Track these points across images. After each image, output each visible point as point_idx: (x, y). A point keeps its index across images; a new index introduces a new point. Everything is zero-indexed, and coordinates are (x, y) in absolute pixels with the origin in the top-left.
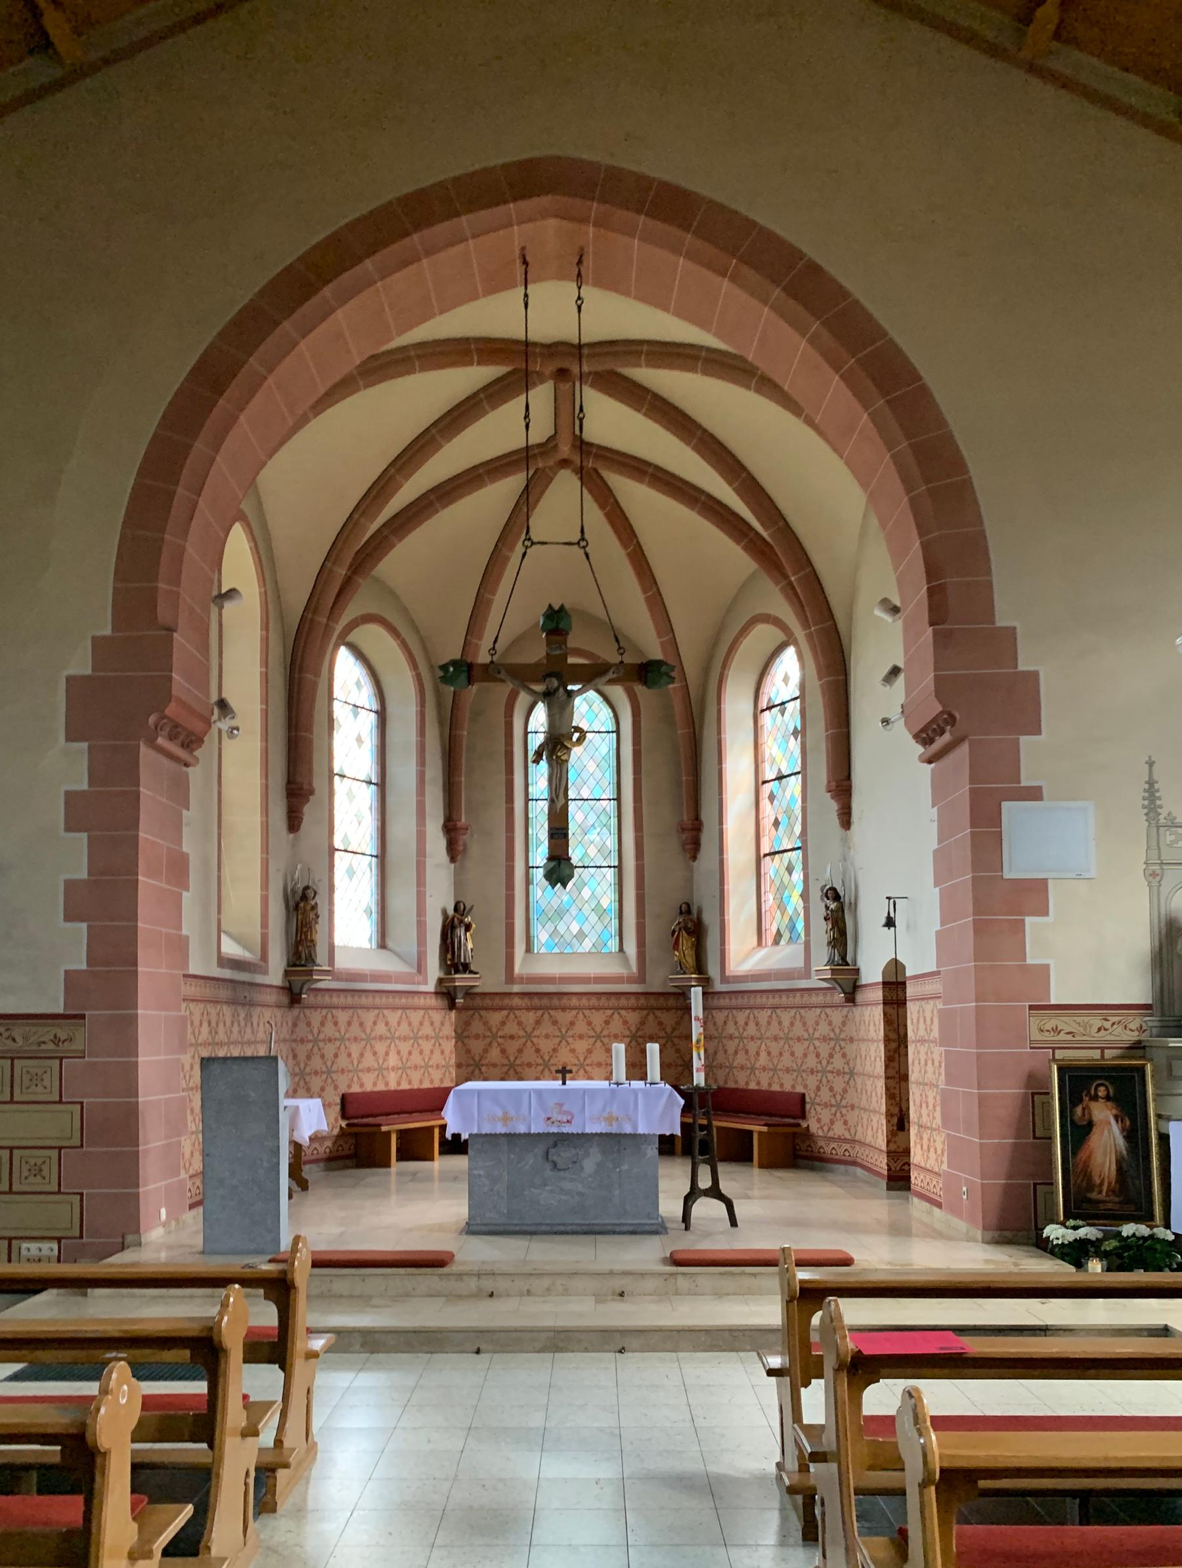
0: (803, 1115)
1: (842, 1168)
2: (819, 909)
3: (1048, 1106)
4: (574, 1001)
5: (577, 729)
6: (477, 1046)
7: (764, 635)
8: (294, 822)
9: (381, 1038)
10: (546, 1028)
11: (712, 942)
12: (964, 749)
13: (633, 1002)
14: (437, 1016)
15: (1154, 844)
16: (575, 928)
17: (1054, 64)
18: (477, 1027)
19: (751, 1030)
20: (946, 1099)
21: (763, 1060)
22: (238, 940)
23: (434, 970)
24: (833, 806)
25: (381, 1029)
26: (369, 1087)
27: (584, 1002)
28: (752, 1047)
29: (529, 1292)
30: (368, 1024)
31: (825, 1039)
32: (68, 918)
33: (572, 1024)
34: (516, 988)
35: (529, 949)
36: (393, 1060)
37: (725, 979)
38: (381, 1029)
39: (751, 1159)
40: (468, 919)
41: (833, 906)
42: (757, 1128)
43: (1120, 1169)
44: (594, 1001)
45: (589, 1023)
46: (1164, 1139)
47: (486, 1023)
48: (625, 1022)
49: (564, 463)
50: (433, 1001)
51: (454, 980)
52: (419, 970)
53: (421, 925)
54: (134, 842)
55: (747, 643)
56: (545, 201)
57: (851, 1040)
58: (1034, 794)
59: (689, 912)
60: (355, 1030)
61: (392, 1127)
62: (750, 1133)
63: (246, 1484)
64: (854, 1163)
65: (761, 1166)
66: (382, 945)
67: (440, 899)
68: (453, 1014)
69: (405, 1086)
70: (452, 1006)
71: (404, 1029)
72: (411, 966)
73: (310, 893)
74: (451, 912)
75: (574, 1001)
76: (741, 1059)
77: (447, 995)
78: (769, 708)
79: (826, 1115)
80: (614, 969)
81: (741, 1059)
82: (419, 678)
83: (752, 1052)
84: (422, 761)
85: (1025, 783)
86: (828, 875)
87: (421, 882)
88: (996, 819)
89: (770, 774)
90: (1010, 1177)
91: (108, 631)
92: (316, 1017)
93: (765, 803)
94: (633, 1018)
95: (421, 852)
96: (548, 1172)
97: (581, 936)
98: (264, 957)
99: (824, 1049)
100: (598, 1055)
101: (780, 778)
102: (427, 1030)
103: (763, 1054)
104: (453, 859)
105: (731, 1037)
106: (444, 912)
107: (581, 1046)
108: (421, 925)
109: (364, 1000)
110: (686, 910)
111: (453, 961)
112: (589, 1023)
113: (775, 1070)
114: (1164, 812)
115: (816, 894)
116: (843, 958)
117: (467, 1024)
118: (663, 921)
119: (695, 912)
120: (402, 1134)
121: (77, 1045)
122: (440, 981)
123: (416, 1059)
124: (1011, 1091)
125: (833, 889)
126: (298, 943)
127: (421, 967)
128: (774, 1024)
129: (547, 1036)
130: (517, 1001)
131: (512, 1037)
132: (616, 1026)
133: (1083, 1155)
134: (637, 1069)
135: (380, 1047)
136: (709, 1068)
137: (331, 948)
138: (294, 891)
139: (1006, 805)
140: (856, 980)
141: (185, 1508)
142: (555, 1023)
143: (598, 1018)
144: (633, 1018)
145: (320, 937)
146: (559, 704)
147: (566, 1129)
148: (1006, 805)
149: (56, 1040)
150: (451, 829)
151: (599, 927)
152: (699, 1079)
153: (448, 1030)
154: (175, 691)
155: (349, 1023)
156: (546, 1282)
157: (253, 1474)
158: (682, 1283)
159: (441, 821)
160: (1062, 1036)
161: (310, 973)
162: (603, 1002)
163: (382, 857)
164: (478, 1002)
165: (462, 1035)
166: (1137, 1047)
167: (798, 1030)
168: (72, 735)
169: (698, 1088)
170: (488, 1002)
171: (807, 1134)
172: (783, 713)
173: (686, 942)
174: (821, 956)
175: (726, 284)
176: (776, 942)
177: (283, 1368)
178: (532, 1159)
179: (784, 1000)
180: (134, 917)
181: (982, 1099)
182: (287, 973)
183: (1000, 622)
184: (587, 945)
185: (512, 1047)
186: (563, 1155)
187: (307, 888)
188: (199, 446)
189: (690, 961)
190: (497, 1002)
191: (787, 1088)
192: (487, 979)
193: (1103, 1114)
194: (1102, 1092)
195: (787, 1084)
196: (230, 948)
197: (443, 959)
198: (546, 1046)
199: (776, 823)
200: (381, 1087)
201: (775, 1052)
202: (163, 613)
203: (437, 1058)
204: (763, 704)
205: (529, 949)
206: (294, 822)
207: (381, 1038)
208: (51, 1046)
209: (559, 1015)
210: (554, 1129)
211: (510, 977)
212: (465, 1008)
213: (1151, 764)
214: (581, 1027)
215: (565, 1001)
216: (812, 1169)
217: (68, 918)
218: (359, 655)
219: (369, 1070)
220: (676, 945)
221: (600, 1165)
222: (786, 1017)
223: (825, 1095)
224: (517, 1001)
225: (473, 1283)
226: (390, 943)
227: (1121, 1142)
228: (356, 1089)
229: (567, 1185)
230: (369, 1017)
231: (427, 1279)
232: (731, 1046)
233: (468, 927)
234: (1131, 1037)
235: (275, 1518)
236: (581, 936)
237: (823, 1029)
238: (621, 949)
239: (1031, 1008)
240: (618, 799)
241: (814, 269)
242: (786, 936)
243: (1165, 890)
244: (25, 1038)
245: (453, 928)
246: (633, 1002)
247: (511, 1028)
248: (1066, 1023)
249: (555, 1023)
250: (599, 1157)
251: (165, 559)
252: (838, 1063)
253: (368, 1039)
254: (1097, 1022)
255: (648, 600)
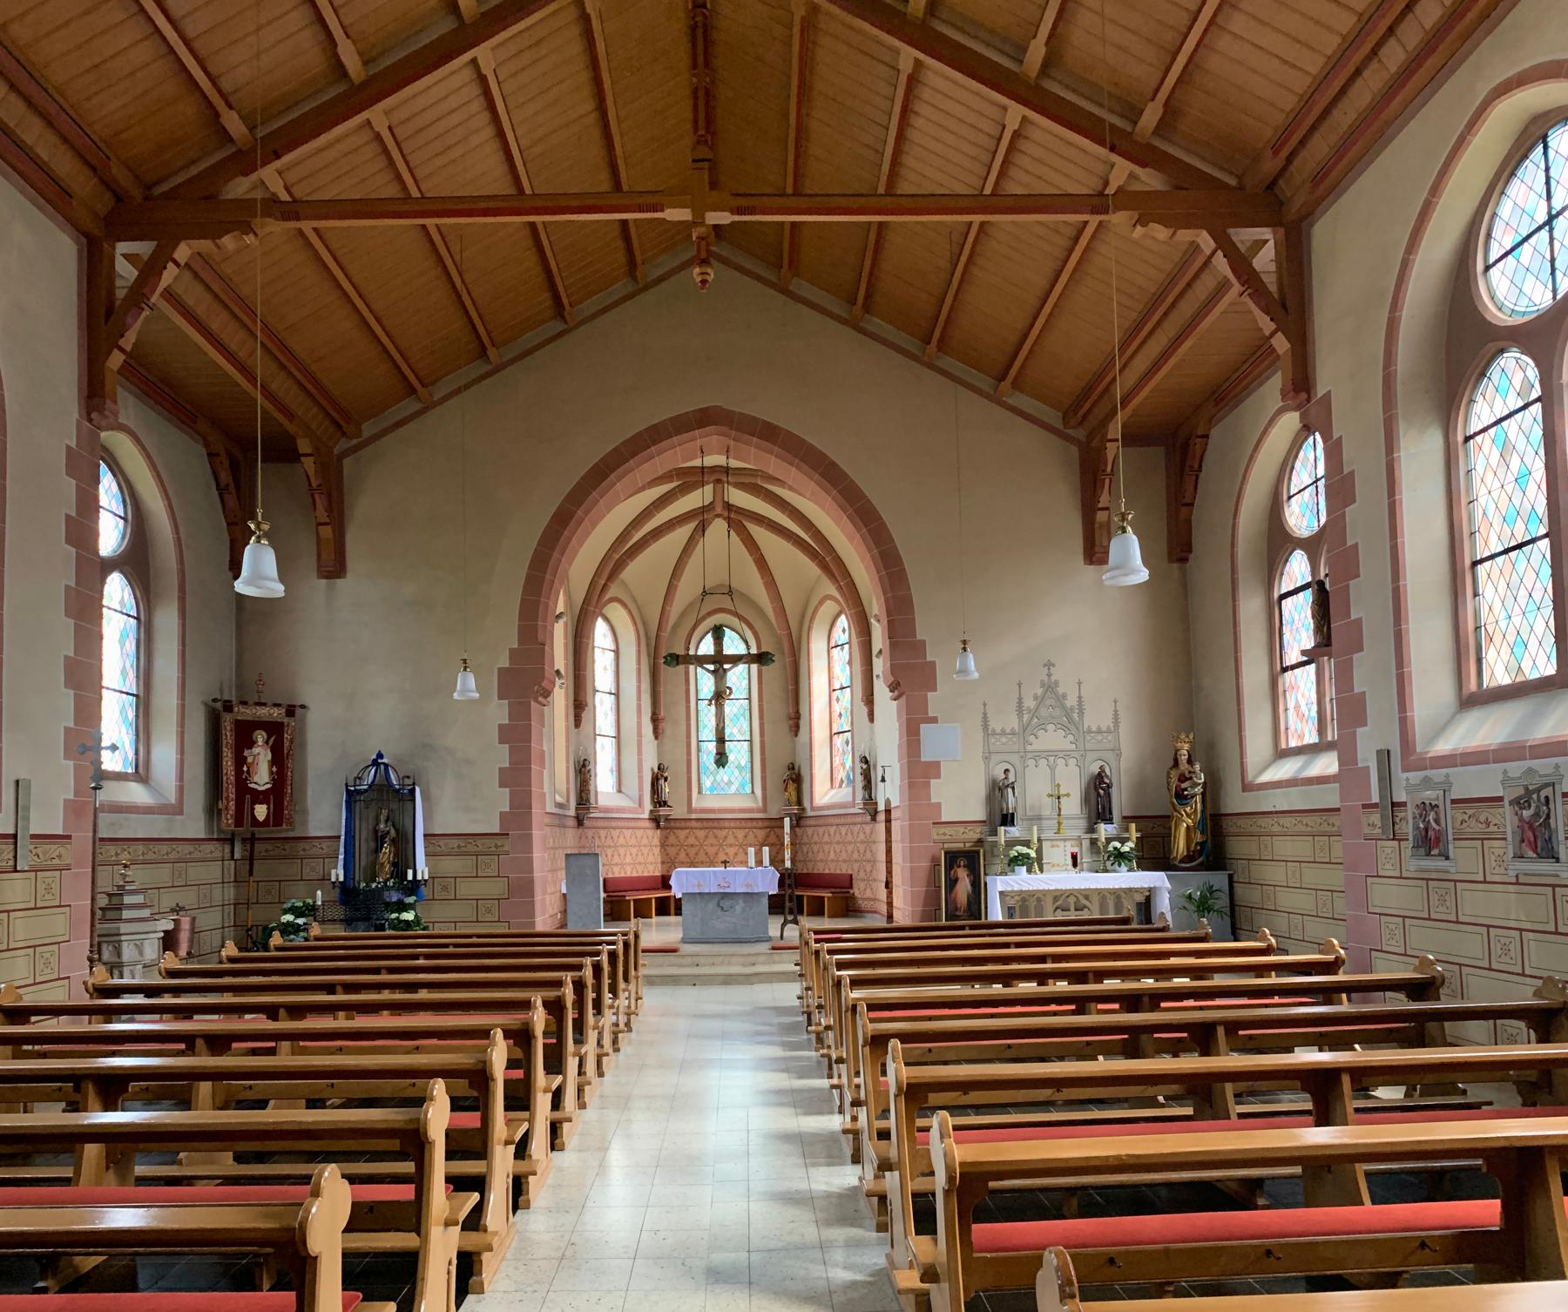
0: (851, 887)
1: (870, 915)
2: (858, 765)
3: (940, 871)
4: (727, 824)
5: (729, 688)
6: (672, 851)
7: (829, 607)
8: (578, 722)
9: (622, 846)
10: (712, 840)
11: (806, 786)
12: (904, 697)
13: (760, 824)
14: (650, 833)
15: (986, 743)
16: (726, 779)
17: (940, 363)
18: (672, 840)
19: (826, 838)
20: (903, 868)
21: (832, 855)
22: (560, 795)
23: (648, 806)
24: (865, 710)
25: (622, 841)
26: (617, 875)
27: (732, 824)
28: (826, 848)
29: (713, 964)
30: (615, 838)
31: (862, 842)
32: (500, 786)
33: (726, 837)
34: (694, 816)
35: (700, 792)
36: (628, 860)
37: (813, 808)
38: (622, 841)
39: (824, 914)
40: (666, 775)
41: (865, 767)
42: (826, 894)
43: (968, 899)
44: (738, 824)
45: (736, 837)
46: (986, 884)
47: (677, 837)
48: (756, 837)
49: (718, 516)
50: (648, 824)
51: (659, 811)
52: (640, 806)
53: (641, 778)
54: (529, 748)
55: (822, 609)
56: (712, 428)
57: (875, 842)
58: (934, 720)
59: (793, 768)
60: (609, 842)
61: (631, 897)
62: (824, 897)
63: (449, 1273)
64: (876, 912)
65: (829, 917)
66: (619, 791)
67: (650, 763)
68: (659, 831)
69: (635, 875)
70: (658, 827)
71: (633, 841)
72: (634, 802)
73: (587, 763)
74: (656, 770)
75: (727, 824)
76: (821, 856)
77: (655, 820)
78: (836, 647)
79: (862, 885)
80: (748, 804)
81: (821, 856)
82: (637, 630)
83: (826, 851)
84: (639, 681)
85: (930, 714)
86: (862, 749)
87: (640, 753)
88: (917, 733)
89: (837, 686)
90: (924, 906)
91: (516, 646)
92: (590, 833)
93: (834, 702)
94: (761, 834)
95: (640, 735)
96: (720, 912)
97: (730, 783)
98: (568, 801)
99: (862, 848)
100: (741, 857)
101: (842, 688)
102: (645, 841)
103: (832, 852)
104: (656, 738)
105: (816, 843)
106: (652, 770)
107: (731, 851)
108: (641, 778)
109: (614, 824)
110: (792, 767)
111: (659, 801)
112: (736, 837)
113: (838, 861)
114: (990, 728)
115: (857, 760)
116: (870, 797)
117: (667, 837)
118: (778, 773)
119: (796, 767)
120: (635, 901)
121: (506, 848)
122: (651, 811)
123: (640, 859)
124: (925, 864)
125: (865, 757)
126: (581, 791)
127: (641, 804)
128: (838, 834)
129: (712, 845)
130: (694, 824)
131: (692, 846)
132: (751, 838)
133: (953, 895)
134: (759, 862)
135: (622, 851)
136: (793, 860)
137: (596, 792)
138: (579, 762)
139: (922, 726)
140: (876, 809)
141: (469, 1198)
142: (716, 837)
143: (740, 834)
144: (761, 834)
145: (592, 788)
146: (719, 674)
147: (728, 890)
148: (922, 726)
149: (496, 846)
150: (655, 720)
151: (740, 778)
152: (788, 864)
153: (656, 842)
154: (546, 675)
155: (606, 837)
156: (721, 959)
157: (455, 1262)
158: (776, 958)
159: (650, 715)
160: (947, 837)
161: (588, 809)
162: (743, 824)
163: (618, 737)
164: (673, 824)
165: (663, 845)
166: (980, 842)
167: (849, 837)
168: (500, 697)
169: (787, 869)
170: (678, 825)
171: (853, 897)
172: (842, 649)
173: (792, 787)
174: (860, 794)
175: (794, 469)
176: (840, 786)
177: (419, 1235)
178: (711, 906)
179: (842, 820)
180: (530, 786)
181: (912, 868)
182: (577, 809)
183: (919, 637)
184: (733, 789)
185: (692, 852)
186: (726, 903)
187: (585, 760)
188: (556, 554)
189: (794, 798)
190: (683, 824)
191: (844, 872)
192: (677, 811)
193: (962, 874)
194: (962, 864)
195: (844, 869)
196: (559, 799)
197: (652, 798)
198: (711, 851)
199: (840, 715)
200: (623, 875)
201: (838, 851)
202: (540, 638)
203: (651, 859)
204: (833, 644)
205: (700, 792)
206: (578, 722)
207: (622, 846)
208: (494, 849)
209: (718, 832)
210: (722, 891)
211: (690, 810)
212: (666, 828)
213: (985, 705)
214: (731, 840)
215: (722, 824)
216: (856, 917)
217: (500, 786)
218: (606, 619)
219: (616, 864)
220: (786, 790)
221: (743, 909)
222: (843, 830)
223: (862, 875)
224: (694, 824)
225: (689, 960)
226: (623, 789)
227: (969, 887)
228: (610, 876)
229: (728, 919)
230: (615, 833)
231: (670, 958)
232: (816, 848)
233: (666, 779)
234: (977, 836)
235: (528, 1213)
236: (730, 783)
237: (862, 836)
238: (753, 792)
239: (934, 823)
240: (749, 699)
241: (833, 464)
242: (845, 782)
243: (991, 765)
244: (483, 845)
245: (658, 779)
246: (760, 824)
247: (691, 840)
248: (949, 830)
249: (716, 837)
250: (743, 905)
251: (541, 607)
252: (868, 856)
253: (616, 846)
254: (962, 830)
255: (765, 583)
